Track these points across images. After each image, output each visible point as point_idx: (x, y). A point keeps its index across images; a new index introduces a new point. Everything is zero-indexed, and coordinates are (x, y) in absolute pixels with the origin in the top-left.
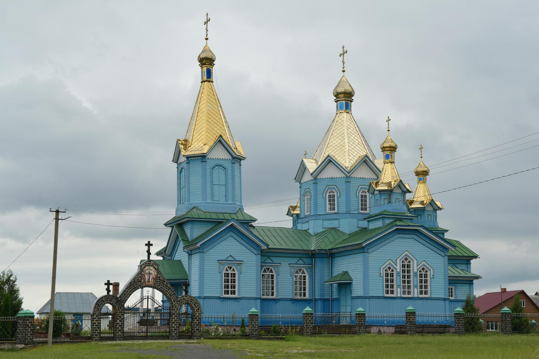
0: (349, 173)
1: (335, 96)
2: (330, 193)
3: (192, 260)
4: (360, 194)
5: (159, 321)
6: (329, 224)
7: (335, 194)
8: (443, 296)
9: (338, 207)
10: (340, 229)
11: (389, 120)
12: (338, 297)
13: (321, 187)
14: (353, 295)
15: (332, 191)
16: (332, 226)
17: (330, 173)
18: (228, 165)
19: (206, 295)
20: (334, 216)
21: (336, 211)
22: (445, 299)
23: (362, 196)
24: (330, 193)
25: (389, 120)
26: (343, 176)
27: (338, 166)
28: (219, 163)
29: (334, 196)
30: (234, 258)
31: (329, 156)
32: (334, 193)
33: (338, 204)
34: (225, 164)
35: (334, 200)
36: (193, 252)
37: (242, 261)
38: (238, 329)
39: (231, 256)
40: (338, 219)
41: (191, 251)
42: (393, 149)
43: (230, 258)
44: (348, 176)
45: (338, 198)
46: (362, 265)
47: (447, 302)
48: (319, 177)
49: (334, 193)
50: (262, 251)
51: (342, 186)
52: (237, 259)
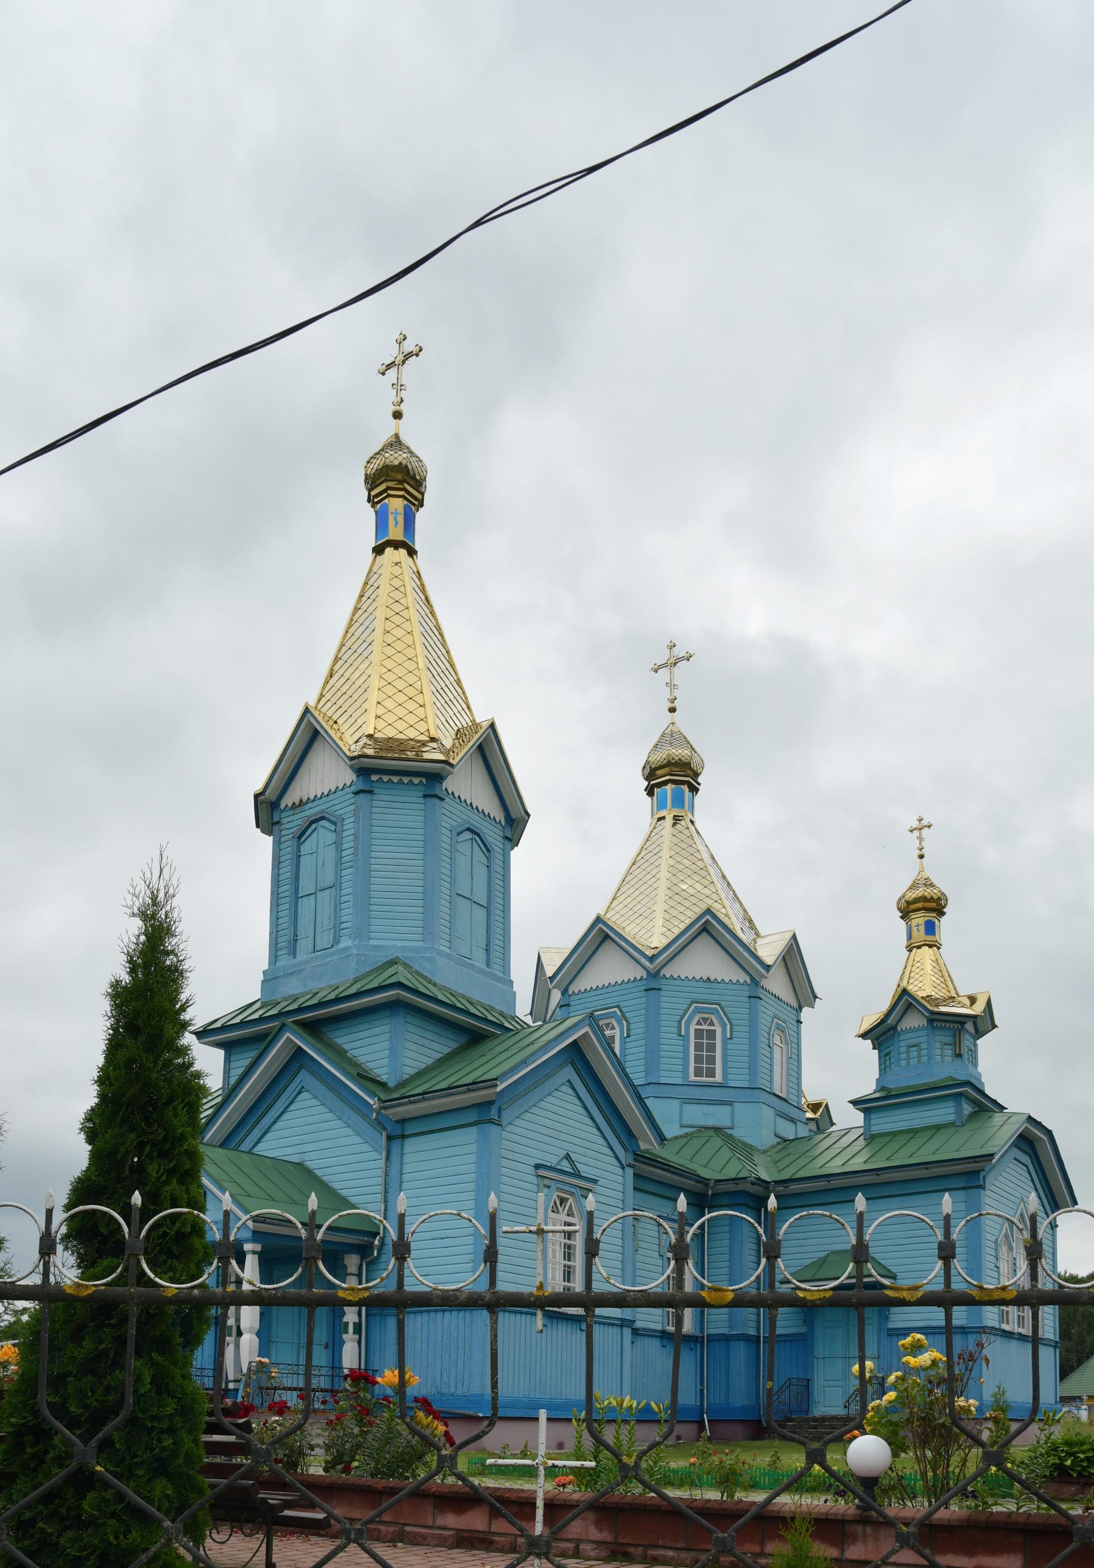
0: (652, 959)
1: (646, 779)
2: (699, 1023)
3: (407, 1158)
4: (693, 1027)
5: (249, 1316)
7: (718, 1029)
10: (736, 1133)
12: (803, 1330)
13: (671, 1003)
14: (891, 1325)
15: (705, 1020)
16: (711, 1123)
17: (609, 971)
18: (493, 836)
20: (715, 1094)
21: (718, 1078)
23: (699, 1033)
24: (699, 1023)
26: (743, 977)
27: (630, 950)
29: (712, 1034)
31: (708, 911)
33: (686, 1058)
37: (595, 1181)
38: (317, 1405)
39: (568, 1157)
40: (730, 1103)
41: (403, 1122)
42: (935, 906)
43: (566, 1166)
44: (655, 973)
45: (725, 1041)
48: (574, 988)
50: (641, 1158)
51: (635, 1005)
52: (584, 1170)
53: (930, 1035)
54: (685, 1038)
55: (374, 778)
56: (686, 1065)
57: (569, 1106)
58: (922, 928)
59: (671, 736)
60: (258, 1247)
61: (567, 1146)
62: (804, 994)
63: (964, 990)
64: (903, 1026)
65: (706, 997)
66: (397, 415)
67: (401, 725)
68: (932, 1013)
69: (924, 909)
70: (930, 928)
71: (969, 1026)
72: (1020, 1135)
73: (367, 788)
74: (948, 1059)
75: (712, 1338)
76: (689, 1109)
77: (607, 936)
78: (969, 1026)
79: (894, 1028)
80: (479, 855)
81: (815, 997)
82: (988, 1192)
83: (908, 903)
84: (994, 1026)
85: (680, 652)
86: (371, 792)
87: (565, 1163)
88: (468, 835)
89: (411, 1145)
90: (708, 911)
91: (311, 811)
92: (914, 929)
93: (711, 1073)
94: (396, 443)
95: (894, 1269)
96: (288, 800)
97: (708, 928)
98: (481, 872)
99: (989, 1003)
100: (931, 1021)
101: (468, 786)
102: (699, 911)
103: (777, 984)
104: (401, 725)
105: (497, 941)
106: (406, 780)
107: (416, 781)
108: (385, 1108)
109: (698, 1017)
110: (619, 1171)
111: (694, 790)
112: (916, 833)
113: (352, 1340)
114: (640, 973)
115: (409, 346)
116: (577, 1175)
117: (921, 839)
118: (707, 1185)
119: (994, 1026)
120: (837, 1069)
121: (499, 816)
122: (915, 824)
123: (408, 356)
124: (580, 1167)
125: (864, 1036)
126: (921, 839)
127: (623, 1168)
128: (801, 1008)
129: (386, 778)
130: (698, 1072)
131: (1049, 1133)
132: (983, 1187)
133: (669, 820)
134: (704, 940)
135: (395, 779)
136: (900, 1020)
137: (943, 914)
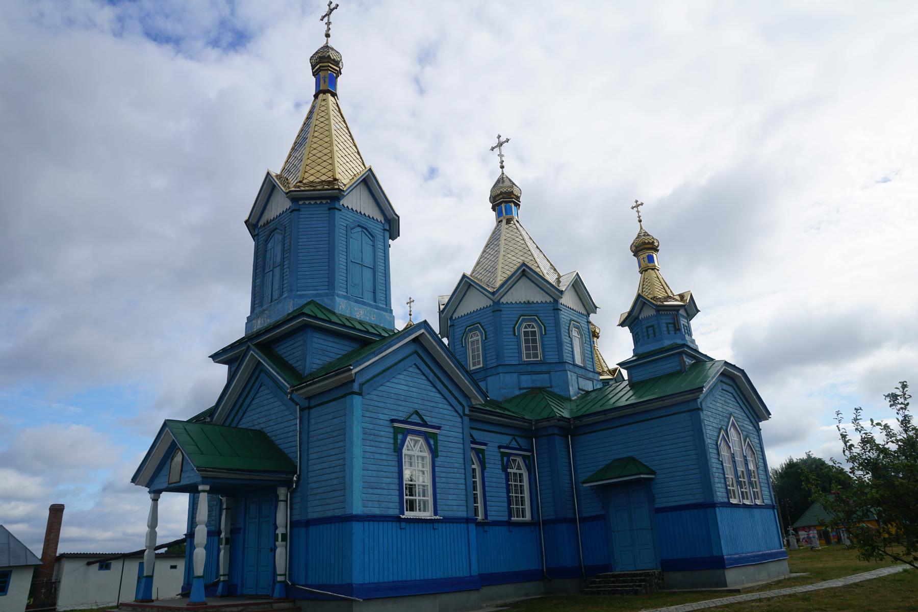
0: (493, 293)
2: (526, 328)
6: (527, 381)
8: (464, 515)
9: (544, 351)
11: (411, 302)
14: (657, 506)
15: (529, 326)
16: (539, 385)
18: (377, 230)
19: (313, 515)
22: (467, 521)
23: (526, 333)
24: (526, 328)
25: (411, 302)
26: (549, 299)
28: (363, 221)
29: (534, 333)
30: (422, 419)
31: (524, 264)
32: (533, 327)
34: (370, 225)
35: (534, 341)
36: (313, 403)
39: (417, 413)
40: (548, 372)
41: (309, 398)
43: (415, 419)
46: (311, 480)
47: (472, 527)
49: (533, 327)
53: (660, 321)
54: (518, 337)
55: (301, 203)
56: (520, 352)
57: (419, 381)
58: (646, 260)
59: (501, 180)
60: (207, 488)
61: (416, 406)
62: (589, 307)
63: (677, 292)
64: (642, 316)
65: (528, 310)
66: (328, 36)
67: (318, 175)
68: (657, 306)
69: (644, 248)
70: (651, 259)
71: (682, 312)
72: (722, 374)
73: (297, 208)
74: (672, 333)
75: (545, 522)
76: (524, 378)
77: (471, 285)
78: (682, 312)
79: (637, 318)
80: (367, 240)
81: (596, 307)
82: (705, 412)
83: (637, 247)
84: (698, 311)
85: (503, 139)
86: (299, 210)
87: (414, 416)
88: (359, 229)
89: (314, 413)
90: (524, 264)
91: (271, 226)
92: (642, 261)
93: (536, 356)
94: (326, 47)
95: (653, 468)
96: (261, 223)
97: (525, 273)
98: (368, 249)
99: (691, 296)
100: (658, 311)
101: (357, 202)
102: (518, 265)
103: (568, 300)
104: (318, 175)
105: (380, 287)
106: (318, 202)
107: (324, 202)
108: (296, 390)
109: (525, 324)
110: (459, 420)
111: (517, 205)
112: (635, 209)
113: (281, 546)
114: (490, 303)
115: (333, 6)
116: (425, 424)
117: (638, 212)
118: (531, 423)
119: (698, 311)
120: (617, 347)
121: (380, 218)
122: (634, 204)
123: (332, 10)
124: (427, 419)
125: (622, 324)
126: (638, 212)
127: (461, 417)
128: (589, 315)
129: (307, 202)
130: (528, 356)
131: (742, 371)
132: (701, 409)
133: (504, 222)
134: (524, 282)
135: (312, 202)
136: (640, 313)
137: (658, 251)
